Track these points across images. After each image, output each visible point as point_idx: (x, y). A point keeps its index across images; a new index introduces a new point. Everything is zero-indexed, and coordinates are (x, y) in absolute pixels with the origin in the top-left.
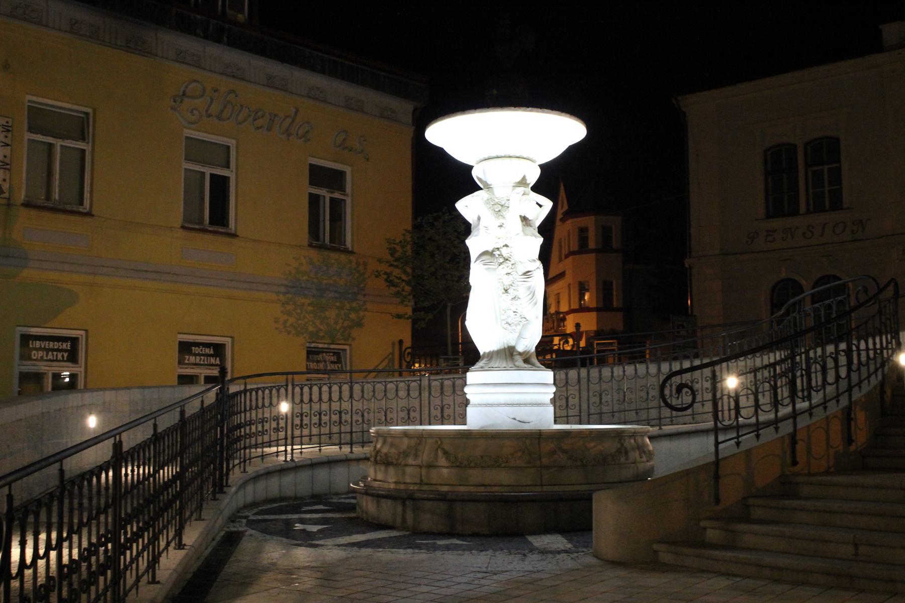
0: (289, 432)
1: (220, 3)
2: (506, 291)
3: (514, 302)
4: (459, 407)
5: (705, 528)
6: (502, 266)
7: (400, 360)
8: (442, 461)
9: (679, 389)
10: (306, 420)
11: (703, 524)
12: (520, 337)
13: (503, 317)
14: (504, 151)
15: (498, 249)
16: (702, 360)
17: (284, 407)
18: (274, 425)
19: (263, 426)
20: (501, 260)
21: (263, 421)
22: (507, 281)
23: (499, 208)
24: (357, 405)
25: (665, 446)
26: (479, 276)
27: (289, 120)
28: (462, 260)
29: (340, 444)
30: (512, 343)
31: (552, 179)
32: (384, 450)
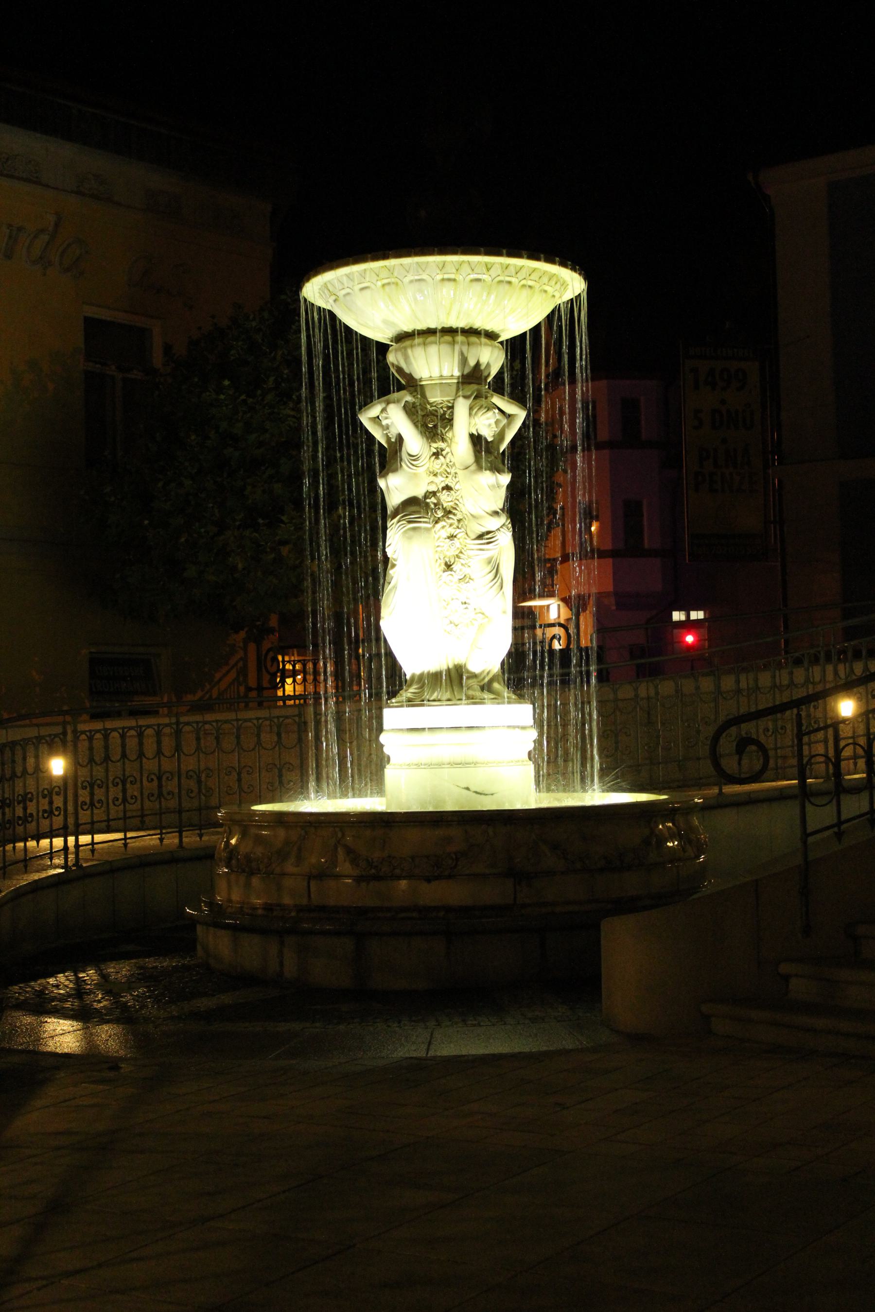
0: (70, 809)
2: (448, 566)
3: (463, 585)
4: (370, 766)
5: (786, 978)
6: (441, 524)
7: (259, 670)
8: (344, 867)
9: (743, 744)
10: (99, 794)
11: (784, 968)
14: (444, 311)
15: (434, 494)
16: (721, 793)
17: (57, 766)
18: (44, 804)
19: (25, 809)
21: (25, 799)
22: (449, 550)
23: (433, 423)
24: (190, 763)
25: (728, 821)
26: (405, 548)
27: (45, 237)
28: (374, 516)
29: (160, 827)
30: (459, 660)
32: (243, 850)
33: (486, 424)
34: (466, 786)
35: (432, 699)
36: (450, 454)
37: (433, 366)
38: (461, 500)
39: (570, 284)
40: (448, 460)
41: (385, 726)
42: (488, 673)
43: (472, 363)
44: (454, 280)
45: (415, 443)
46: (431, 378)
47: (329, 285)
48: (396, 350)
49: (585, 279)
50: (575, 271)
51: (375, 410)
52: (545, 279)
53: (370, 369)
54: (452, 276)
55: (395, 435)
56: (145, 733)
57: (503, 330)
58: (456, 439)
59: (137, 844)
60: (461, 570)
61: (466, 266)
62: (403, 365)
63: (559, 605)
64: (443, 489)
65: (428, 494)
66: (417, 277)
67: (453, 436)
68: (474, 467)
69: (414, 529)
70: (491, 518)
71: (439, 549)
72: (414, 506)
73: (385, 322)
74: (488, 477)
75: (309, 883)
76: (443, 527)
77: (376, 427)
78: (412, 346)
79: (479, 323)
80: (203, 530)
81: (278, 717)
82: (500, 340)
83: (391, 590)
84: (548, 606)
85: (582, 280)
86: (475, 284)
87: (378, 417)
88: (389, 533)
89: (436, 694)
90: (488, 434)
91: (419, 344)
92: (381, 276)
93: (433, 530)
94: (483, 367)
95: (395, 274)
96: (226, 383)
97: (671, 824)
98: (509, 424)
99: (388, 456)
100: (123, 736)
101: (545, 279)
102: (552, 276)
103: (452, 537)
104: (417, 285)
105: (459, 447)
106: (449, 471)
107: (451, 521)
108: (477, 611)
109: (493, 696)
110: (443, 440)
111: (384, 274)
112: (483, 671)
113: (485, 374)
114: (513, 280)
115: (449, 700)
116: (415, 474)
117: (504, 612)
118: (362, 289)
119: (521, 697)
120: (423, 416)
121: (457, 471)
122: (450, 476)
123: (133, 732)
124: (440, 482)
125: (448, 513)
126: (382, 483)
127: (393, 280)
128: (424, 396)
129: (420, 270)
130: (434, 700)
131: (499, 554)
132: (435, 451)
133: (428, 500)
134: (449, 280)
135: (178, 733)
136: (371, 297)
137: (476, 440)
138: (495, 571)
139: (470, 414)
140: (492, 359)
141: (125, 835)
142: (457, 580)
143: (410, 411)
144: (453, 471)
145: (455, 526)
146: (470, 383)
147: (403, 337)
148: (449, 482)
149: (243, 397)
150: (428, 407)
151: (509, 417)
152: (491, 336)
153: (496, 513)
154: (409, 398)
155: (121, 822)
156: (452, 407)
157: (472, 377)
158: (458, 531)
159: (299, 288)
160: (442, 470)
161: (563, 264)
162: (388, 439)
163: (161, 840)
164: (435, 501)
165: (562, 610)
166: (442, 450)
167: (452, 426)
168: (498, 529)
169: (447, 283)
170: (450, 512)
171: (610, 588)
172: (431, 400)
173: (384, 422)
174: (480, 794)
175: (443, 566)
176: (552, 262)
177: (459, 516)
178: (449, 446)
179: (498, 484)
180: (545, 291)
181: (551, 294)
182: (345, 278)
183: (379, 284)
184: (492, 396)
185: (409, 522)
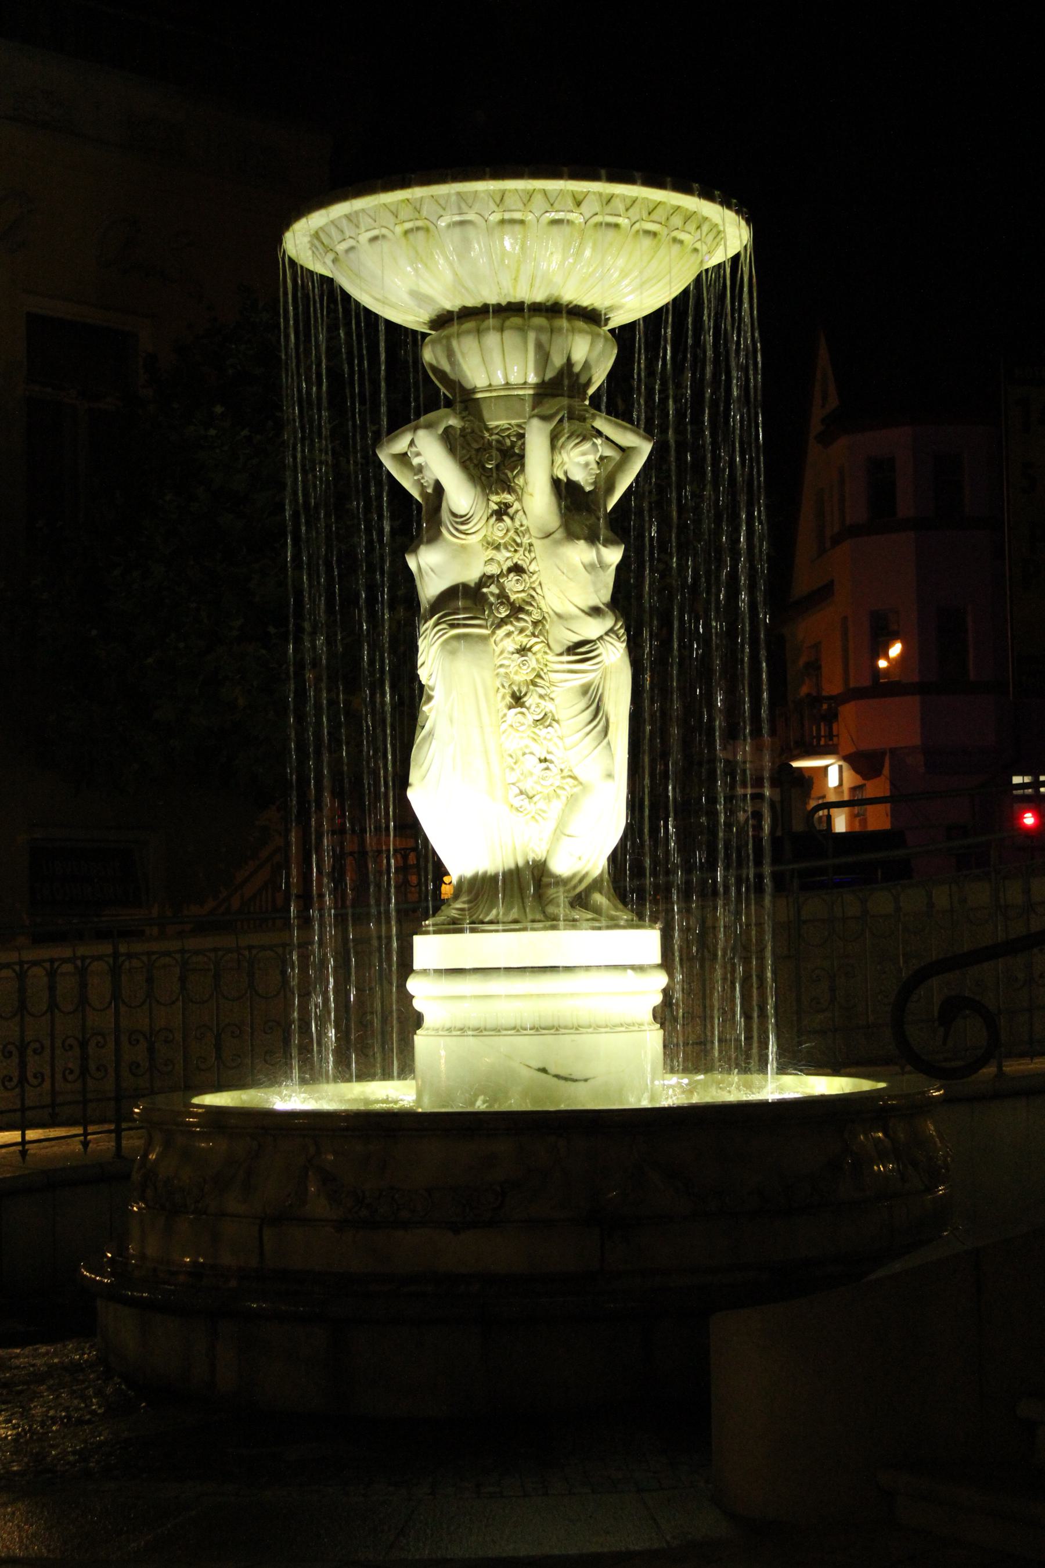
1: (4, 1150)
2: (518, 700)
3: (542, 731)
4: (382, 1031)
12: (559, 832)
13: (513, 777)
20: (504, 612)
22: (521, 673)
23: (493, 464)
28: (405, 609)
30: (537, 852)
31: (656, 366)
33: (579, 463)
34: (541, 1066)
35: (487, 919)
36: (521, 513)
37: (499, 367)
38: (539, 590)
39: (725, 234)
40: (517, 524)
41: (417, 965)
42: (581, 881)
43: (558, 361)
44: (522, 222)
45: (460, 495)
46: (490, 388)
47: (322, 235)
48: (433, 342)
49: (748, 222)
50: (729, 207)
51: (401, 445)
52: (677, 221)
53: (393, 373)
54: (517, 216)
55: (432, 482)
56: (30, 973)
57: (611, 308)
58: (530, 489)
59: (55, 1149)
60: (538, 706)
61: (538, 198)
62: (446, 367)
63: (841, 767)
64: (510, 570)
65: (486, 580)
66: (457, 218)
67: (526, 483)
68: (558, 535)
69: (458, 637)
70: (590, 619)
71: (502, 671)
72: (467, 600)
73: (415, 294)
74: (580, 553)
75: (261, 1231)
76: (509, 634)
77: (406, 471)
78: (459, 335)
79: (572, 294)
80: (182, 645)
81: (250, 948)
82: (612, 325)
83: (424, 739)
84: (826, 768)
85: (743, 223)
86: (555, 229)
87: (406, 454)
88: (422, 644)
89: (494, 912)
90: (581, 476)
91: (468, 332)
92: (402, 215)
93: (492, 640)
94: (577, 369)
95: (424, 213)
96: (219, 409)
97: (880, 1135)
98: (621, 466)
99: (418, 518)
100: (52, 974)
101: (677, 221)
102: (689, 217)
103: (523, 651)
104: (457, 231)
105: (537, 501)
106: (519, 540)
107: (522, 624)
108: (566, 773)
109: (590, 916)
110: (510, 490)
111: (405, 213)
112: (574, 876)
113: (583, 380)
114: (622, 221)
115: (516, 921)
116: (463, 546)
117: (610, 776)
118: (375, 239)
119: (639, 920)
120: (478, 450)
121: (534, 541)
122: (521, 550)
123: (67, 968)
124: (504, 558)
125: (517, 610)
126: (412, 563)
127: (419, 223)
128: (481, 419)
129: (463, 206)
130: (491, 922)
131: (604, 677)
132: (496, 507)
133: (485, 590)
134: (513, 221)
135: (115, 971)
136: (398, 254)
137: (566, 492)
138: (594, 706)
139: (553, 447)
140: (592, 356)
141: (23, 1136)
142: (531, 722)
143: (450, 441)
144: (526, 541)
145: (528, 632)
146: (554, 396)
147: (443, 321)
148: (518, 558)
149: (245, 432)
150: (487, 435)
151: (625, 452)
152: (591, 317)
153: (595, 611)
154: (453, 422)
155: (19, 1114)
156: (522, 436)
157: (559, 393)
158: (534, 640)
159: (279, 240)
160: (507, 539)
161: (707, 195)
162: (424, 493)
163: (85, 1144)
164: (497, 591)
165: (845, 774)
166: (508, 506)
167: (523, 466)
168: (601, 638)
169: (508, 228)
170: (521, 609)
171: (917, 741)
172: (492, 424)
173: (415, 461)
174: (566, 1079)
175: (509, 699)
176: (687, 190)
177: (536, 616)
178: (519, 499)
179: (600, 562)
180: (681, 242)
181: (690, 247)
182: (344, 222)
183: (399, 230)
184: (594, 417)
185: (453, 626)
